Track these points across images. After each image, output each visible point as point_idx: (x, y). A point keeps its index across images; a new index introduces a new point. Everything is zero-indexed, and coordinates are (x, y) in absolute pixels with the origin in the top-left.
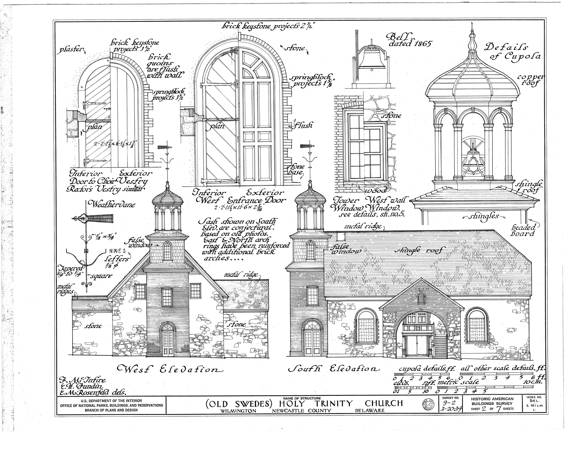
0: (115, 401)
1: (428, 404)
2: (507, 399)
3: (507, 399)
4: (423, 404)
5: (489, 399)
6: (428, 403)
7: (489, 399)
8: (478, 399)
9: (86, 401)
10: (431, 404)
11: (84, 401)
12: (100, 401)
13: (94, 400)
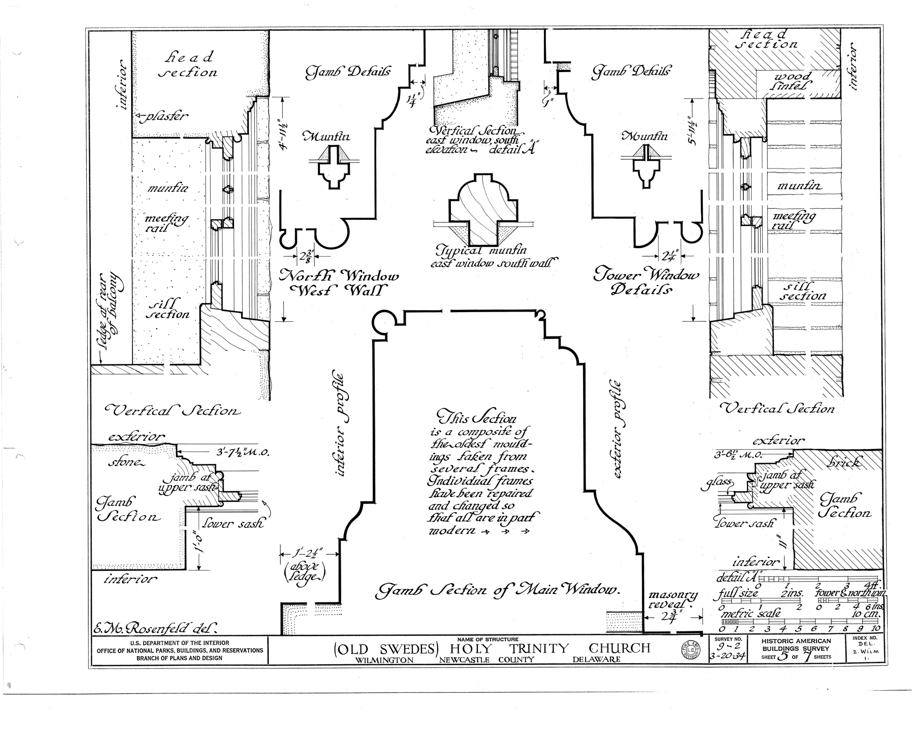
0: (186, 643)
1: (690, 650)
2: (820, 641)
3: (820, 641)
4: (682, 649)
5: (791, 641)
7: (791, 641)
8: (774, 641)
9: (138, 644)
10: (694, 650)
11: (135, 643)
12: (161, 643)
13: (151, 642)
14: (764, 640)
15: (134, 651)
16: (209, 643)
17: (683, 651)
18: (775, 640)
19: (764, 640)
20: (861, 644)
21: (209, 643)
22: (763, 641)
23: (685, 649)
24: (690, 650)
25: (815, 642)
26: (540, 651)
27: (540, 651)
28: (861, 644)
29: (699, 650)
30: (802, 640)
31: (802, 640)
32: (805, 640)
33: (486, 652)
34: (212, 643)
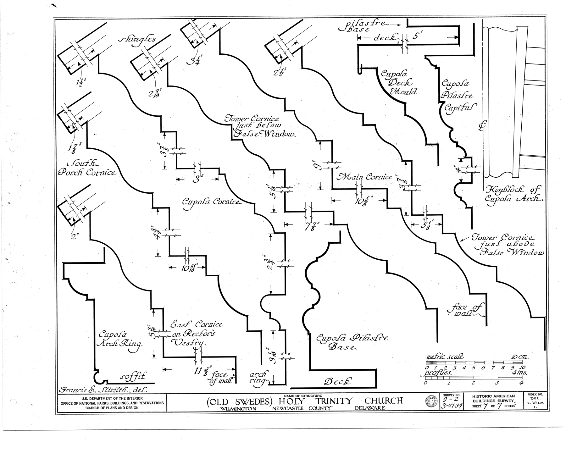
1: (431, 401)
2: (508, 396)
3: (508, 396)
5: (491, 396)
6: (431, 400)
7: (491, 396)
8: (480, 396)
10: (434, 401)
11: (84, 399)
12: (101, 399)
14: (474, 396)
15: (84, 403)
16: (131, 398)
17: (427, 402)
18: (481, 395)
19: (474, 396)
20: (532, 398)
21: (131, 398)
22: (473, 396)
23: (428, 400)
24: (431, 401)
25: (505, 397)
26: (331, 399)
27: (331, 399)
28: (532, 398)
29: (437, 401)
30: (497, 395)
31: (497, 395)
32: (499, 395)
33: (285, 399)
34: (132, 398)
